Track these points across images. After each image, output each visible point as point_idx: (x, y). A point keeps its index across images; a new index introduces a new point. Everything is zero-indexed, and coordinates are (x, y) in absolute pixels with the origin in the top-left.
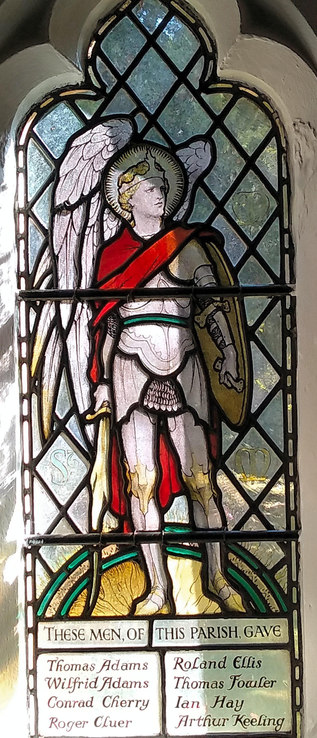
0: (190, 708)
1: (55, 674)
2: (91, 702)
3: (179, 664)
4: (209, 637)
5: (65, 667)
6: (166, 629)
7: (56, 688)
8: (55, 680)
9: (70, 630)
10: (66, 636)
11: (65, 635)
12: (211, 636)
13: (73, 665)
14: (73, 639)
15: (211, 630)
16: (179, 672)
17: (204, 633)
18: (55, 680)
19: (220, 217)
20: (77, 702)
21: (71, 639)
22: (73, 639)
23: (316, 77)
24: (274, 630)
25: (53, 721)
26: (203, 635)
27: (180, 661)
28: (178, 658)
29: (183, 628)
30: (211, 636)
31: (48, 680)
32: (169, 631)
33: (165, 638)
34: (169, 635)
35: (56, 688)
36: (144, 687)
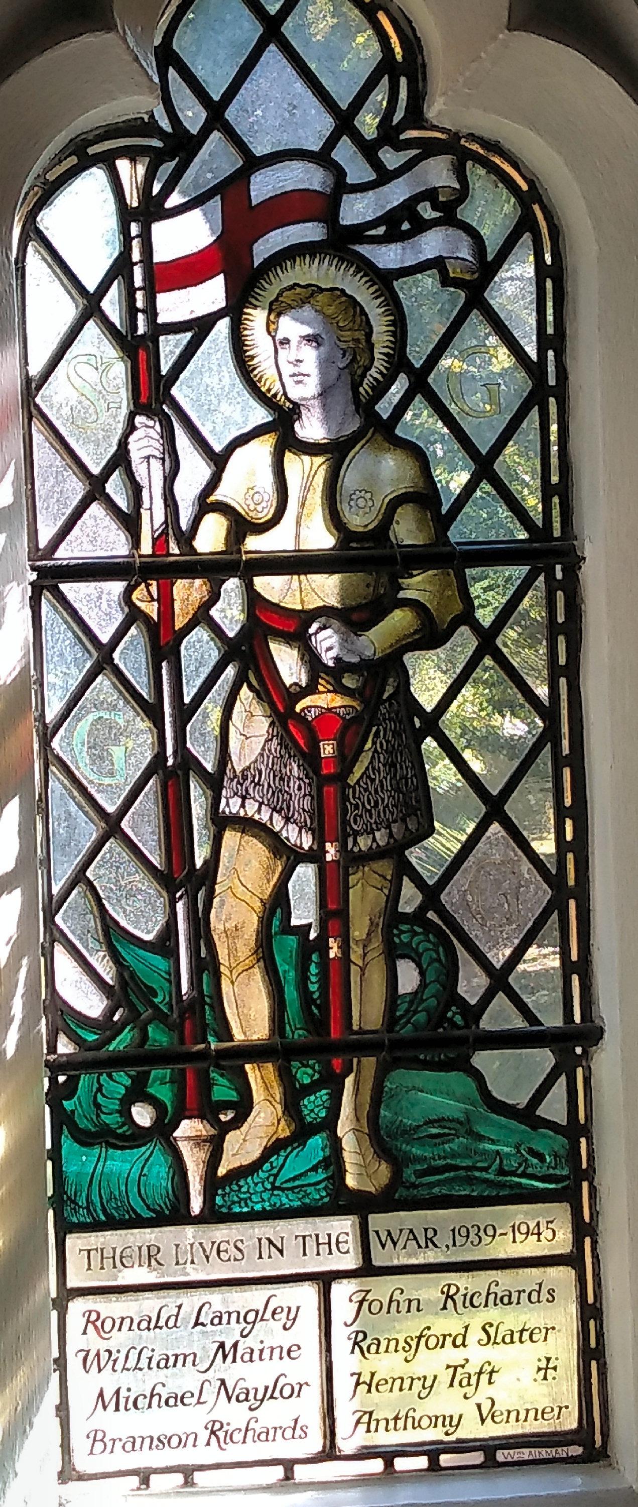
0: (382, 1355)
1: (94, 1342)
2: (464, 1337)
3: (93, 1323)
4: (427, 1247)
5: (139, 1324)
6: (317, 1236)
7: (100, 1370)
8: (98, 1354)
9: (228, 1242)
10: (222, 1254)
11: (338, 1242)
12: (430, 1244)
13: (123, 1319)
14: (235, 1260)
15: (430, 1234)
16: (94, 1342)
17: (415, 1239)
18: (98, 1354)
19: (345, 141)
20: (450, 1335)
21: (232, 1258)
22: (235, 1260)
23: (636, 7)
24: (219, 1252)
25: (96, 1438)
26: (414, 1242)
27: (94, 1316)
28: (90, 1312)
29: (242, 1241)
30: (430, 1244)
31: (83, 1354)
32: (323, 1238)
33: (315, 1252)
34: (108, 1262)
35: (100, 1370)
36: (548, 1300)
